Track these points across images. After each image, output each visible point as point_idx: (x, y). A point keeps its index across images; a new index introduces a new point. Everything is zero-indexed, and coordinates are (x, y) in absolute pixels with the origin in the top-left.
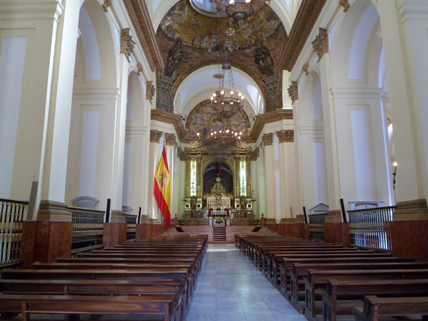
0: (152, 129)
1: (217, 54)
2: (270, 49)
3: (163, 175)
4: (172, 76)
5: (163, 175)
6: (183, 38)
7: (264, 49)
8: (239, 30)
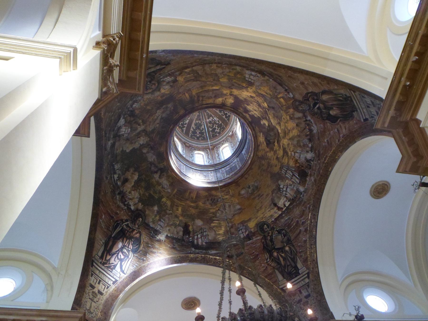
1: (310, 180)
2: (305, 92)
4: (300, 272)
6: (262, 218)
7: (308, 100)
8: (280, 131)
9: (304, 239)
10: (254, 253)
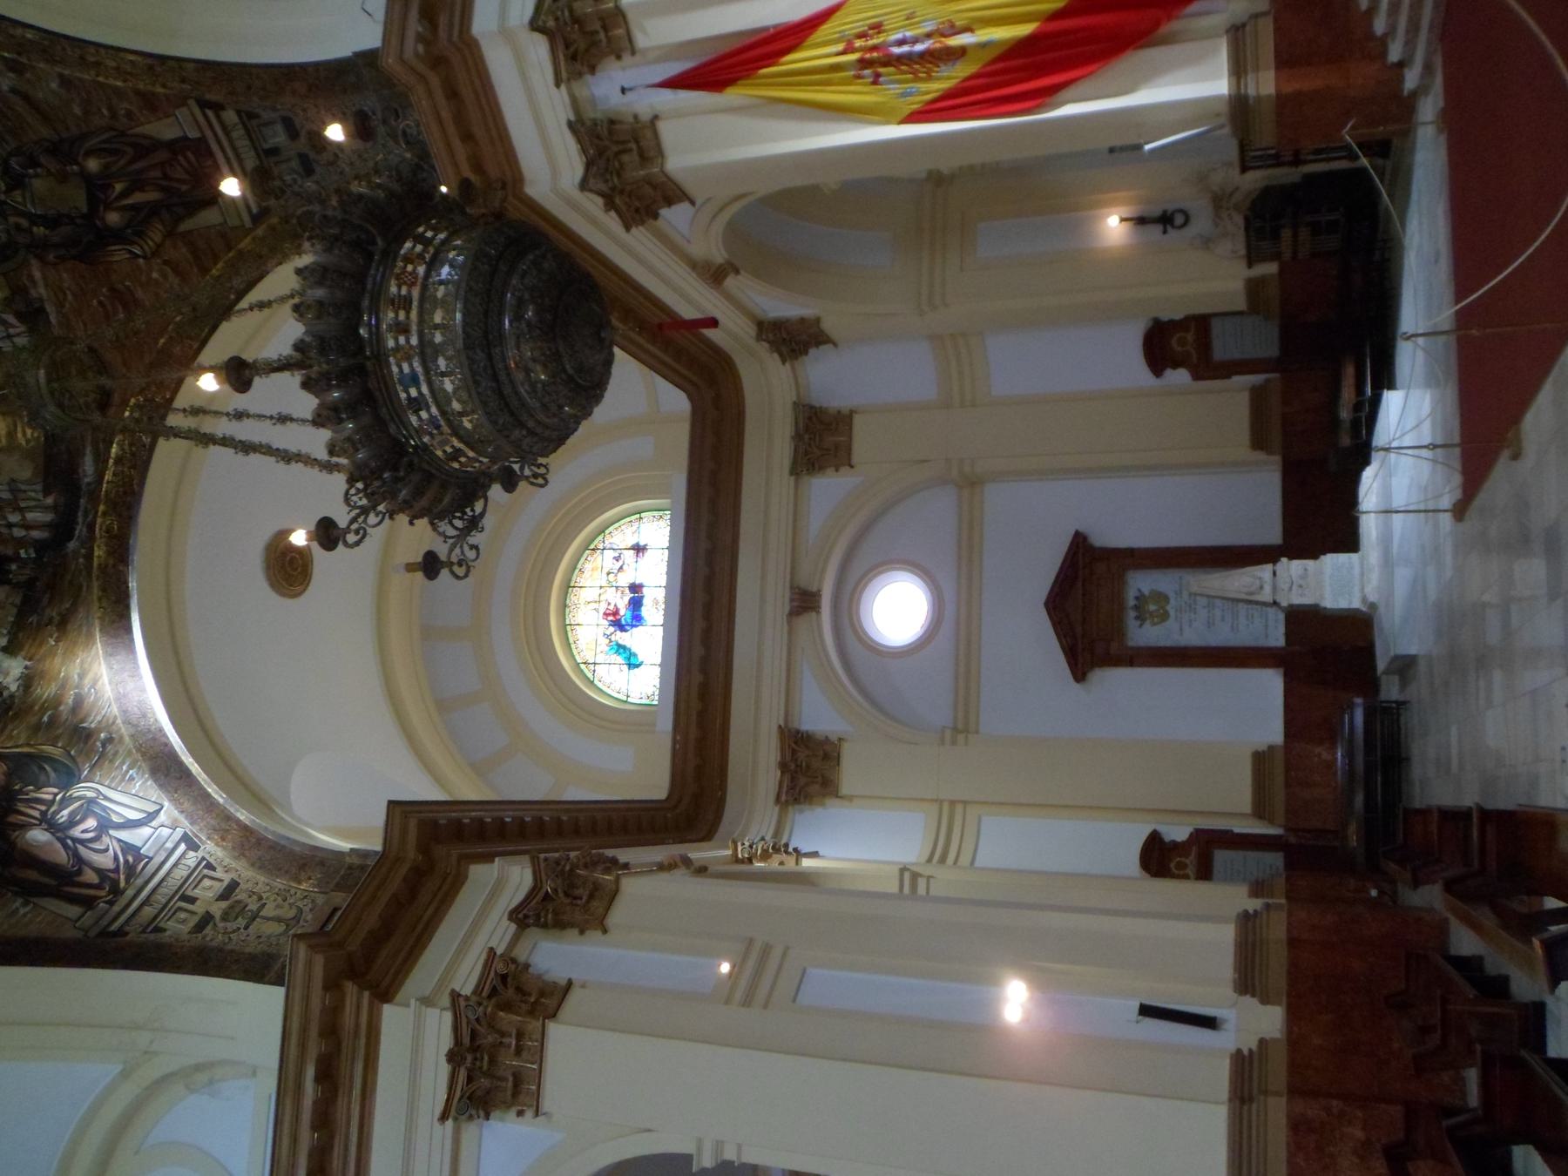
0: (858, 421)
3: (876, 63)
5: (876, 63)
9: (54, 85)
10: (100, 303)
